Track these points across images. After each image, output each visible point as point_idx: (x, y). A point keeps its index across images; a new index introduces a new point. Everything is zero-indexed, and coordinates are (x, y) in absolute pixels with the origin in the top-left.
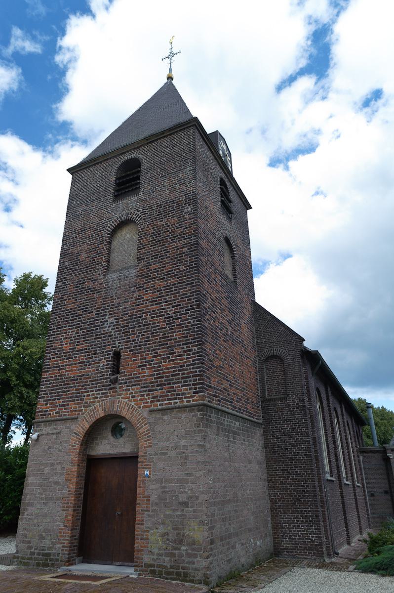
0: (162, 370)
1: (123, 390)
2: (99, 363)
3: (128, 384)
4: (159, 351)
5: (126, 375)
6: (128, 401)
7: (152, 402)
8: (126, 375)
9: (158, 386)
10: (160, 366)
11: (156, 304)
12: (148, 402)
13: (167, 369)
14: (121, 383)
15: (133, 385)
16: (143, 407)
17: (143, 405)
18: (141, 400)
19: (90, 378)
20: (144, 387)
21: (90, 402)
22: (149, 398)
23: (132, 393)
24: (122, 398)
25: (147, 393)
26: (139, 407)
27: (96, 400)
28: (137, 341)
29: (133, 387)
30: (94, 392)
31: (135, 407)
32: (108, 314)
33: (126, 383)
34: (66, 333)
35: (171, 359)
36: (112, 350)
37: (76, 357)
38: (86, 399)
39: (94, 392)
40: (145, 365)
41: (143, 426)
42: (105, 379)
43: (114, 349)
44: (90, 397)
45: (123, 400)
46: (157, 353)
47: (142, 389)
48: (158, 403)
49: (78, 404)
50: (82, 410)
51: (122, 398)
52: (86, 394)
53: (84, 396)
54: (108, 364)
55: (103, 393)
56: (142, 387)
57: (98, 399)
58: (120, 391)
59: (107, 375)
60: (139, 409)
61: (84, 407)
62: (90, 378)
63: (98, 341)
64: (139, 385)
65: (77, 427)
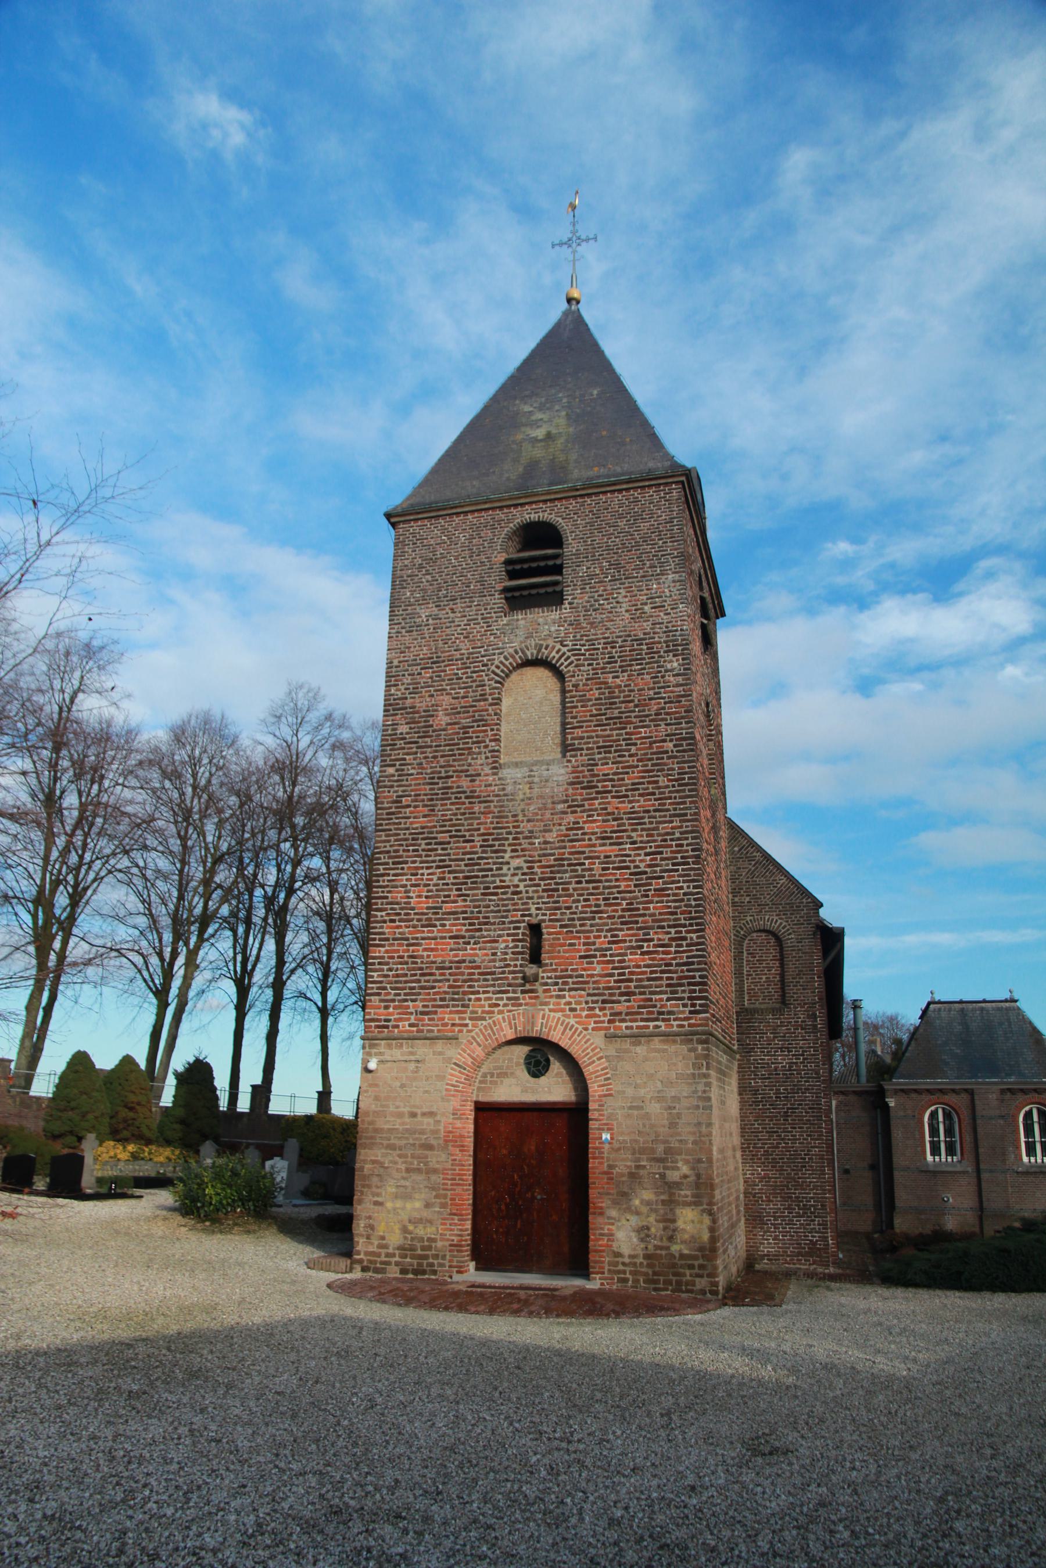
0: (629, 967)
1: (551, 997)
2: (497, 941)
3: (560, 986)
4: (620, 933)
5: (555, 970)
6: (577, 1023)
7: (610, 1021)
8: (555, 970)
9: (622, 994)
10: (624, 961)
11: (611, 844)
12: (603, 1022)
13: (639, 967)
14: (546, 984)
15: (570, 990)
16: (593, 1029)
17: (593, 1025)
18: (587, 1016)
19: (479, 967)
20: (594, 995)
21: (483, 1012)
22: (605, 1015)
23: (570, 1003)
24: (550, 1010)
25: (600, 1004)
26: (586, 1029)
27: (496, 1009)
28: (574, 910)
29: (573, 993)
30: (490, 995)
31: (577, 1029)
32: (509, 849)
33: (556, 984)
34: (417, 874)
35: (645, 949)
36: (524, 921)
37: (444, 925)
38: (473, 1006)
39: (490, 995)
40: (595, 956)
41: (594, 1062)
42: (510, 972)
43: (526, 919)
44: (483, 1002)
45: (552, 1014)
46: (616, 936)
47: (590, 999)
48: (624, 1025)
49: (458, 1012)
50: (466, 1025)
51: (550, 1010)
52: (473, 997)
53: (470, 1000)
54: (516, 947)
55: (508, 999)
56: (589, 995)
57: (501, 1008)
58: (546, 997)
59: (516, 966)
60: (585, 1032)
61: (471, 1019)
62: (479, 967)
63: (490, 900)
64: (584, 989)
65: (460, 1054)
